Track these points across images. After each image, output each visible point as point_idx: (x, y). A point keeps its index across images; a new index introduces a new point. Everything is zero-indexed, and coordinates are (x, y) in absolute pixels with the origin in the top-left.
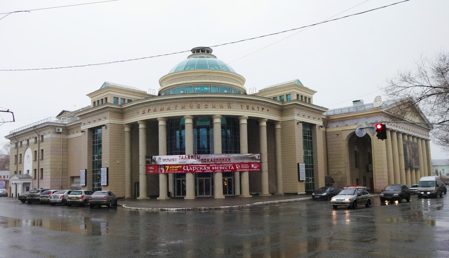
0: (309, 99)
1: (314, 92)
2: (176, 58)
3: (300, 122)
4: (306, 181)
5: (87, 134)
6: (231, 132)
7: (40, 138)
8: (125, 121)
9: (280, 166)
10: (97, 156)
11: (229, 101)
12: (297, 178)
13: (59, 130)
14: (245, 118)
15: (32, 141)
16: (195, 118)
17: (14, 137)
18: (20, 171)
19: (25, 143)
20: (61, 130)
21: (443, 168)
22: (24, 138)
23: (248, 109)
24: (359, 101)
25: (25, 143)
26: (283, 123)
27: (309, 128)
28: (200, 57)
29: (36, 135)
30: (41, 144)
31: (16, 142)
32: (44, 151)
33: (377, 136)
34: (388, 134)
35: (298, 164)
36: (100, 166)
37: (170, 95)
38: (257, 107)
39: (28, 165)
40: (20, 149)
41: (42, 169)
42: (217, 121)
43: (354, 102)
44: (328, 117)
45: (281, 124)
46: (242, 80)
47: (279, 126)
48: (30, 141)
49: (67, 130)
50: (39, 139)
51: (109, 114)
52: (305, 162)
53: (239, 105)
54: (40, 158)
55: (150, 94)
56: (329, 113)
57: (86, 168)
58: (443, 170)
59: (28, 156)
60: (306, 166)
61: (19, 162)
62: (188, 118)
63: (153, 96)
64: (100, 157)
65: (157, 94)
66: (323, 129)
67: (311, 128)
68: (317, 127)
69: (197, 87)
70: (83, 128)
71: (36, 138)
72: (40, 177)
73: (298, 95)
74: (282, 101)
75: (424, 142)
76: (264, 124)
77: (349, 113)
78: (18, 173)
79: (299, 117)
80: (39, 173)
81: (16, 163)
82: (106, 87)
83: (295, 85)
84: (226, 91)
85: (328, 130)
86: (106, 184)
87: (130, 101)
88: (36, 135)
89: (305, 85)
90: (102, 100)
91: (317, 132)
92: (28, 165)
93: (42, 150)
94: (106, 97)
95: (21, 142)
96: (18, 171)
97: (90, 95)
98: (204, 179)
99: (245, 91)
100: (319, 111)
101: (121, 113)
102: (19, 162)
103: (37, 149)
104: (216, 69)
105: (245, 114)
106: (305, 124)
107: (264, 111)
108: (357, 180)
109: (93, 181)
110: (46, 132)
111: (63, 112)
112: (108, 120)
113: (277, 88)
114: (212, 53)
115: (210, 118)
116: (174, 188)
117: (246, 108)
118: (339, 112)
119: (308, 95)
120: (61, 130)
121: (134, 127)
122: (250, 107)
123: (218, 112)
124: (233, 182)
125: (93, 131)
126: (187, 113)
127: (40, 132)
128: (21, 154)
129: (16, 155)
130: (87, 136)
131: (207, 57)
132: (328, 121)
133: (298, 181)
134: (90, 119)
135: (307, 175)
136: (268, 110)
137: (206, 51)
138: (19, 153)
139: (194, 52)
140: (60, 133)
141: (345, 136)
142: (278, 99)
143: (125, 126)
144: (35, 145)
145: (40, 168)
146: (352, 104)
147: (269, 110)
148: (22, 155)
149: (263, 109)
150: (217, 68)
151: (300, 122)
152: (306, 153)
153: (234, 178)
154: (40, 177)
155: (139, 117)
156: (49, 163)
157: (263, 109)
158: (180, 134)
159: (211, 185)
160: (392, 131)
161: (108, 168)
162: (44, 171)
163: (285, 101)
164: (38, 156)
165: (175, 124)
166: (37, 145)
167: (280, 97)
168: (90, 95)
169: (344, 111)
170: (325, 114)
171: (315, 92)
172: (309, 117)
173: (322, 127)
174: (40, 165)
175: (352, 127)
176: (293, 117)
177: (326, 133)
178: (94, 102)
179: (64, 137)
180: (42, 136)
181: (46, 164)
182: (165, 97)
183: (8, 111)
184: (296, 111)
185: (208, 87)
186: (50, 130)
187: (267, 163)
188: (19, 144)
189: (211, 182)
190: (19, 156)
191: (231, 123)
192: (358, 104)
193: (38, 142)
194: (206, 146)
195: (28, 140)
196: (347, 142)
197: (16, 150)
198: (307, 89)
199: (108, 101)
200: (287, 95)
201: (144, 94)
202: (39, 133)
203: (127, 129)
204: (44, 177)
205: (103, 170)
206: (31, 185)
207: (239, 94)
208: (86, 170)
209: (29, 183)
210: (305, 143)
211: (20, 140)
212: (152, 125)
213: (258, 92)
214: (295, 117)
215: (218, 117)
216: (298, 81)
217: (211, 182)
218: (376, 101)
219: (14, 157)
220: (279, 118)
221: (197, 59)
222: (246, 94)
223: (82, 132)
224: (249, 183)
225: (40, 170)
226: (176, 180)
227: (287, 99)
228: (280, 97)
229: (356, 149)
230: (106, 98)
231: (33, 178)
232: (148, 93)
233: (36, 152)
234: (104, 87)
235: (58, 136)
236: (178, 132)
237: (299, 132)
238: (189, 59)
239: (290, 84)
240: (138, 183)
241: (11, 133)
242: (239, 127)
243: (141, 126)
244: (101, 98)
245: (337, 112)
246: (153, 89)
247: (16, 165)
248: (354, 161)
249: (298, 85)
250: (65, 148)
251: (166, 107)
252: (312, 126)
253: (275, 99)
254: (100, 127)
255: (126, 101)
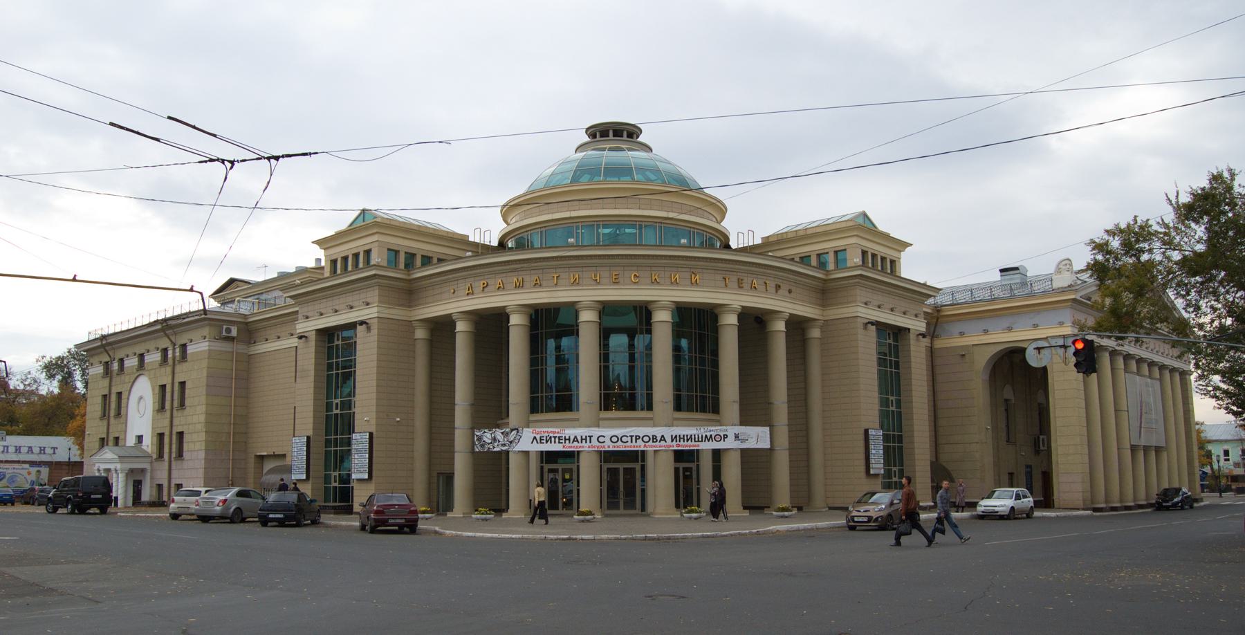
0: (892, 262)
1: (906, 245)
2: (552, 147)
3: (872, 323)
4: (884, 476)
5: (312, 343)
6: (689, 344)
7: (178, 350)
8: (417, 312)
9: (817, 436)
10: (338, 401)
11: (693, 267)
12: (863, 468)
13: (229, 331)
14: (733, 311)
15: (153, 358)
16: (606, 309)
17: (103, 346)
18: (117, 439)
19: (131, 363)
20: (234, 333)
21: (1226, 447)
22: (129, 351)
23: (740, 287)
24: (1017, 269)
25: (131, 363)
26: (826, 325)
27: (892, 336)
28: (611, 149)
29: (164, 343)
30: (178, 368)
31: (107, 359)
32: (188, 385)
33: (1076, 365)
34: (1105, 359)
35: (866, 431)
36: (350, 429)
37: (533, 248)
38: (762, 282)
39: (141, 420)
40: (116, 380)
41: (181, 434)
42: (662, 317)
43: (1001, 271)
44: (938, 309)
45: (821, 327)
46: (720, 209)
47: (815, 333)
48: (148, 359)
49: (249, 331)
50: (174, 352)
51: (377, 292)
52: (882, 427)
53: (719, 277)
54: (176, 404)
55: (477, 240)
56: (941, 299)
57: (310, 433)
58: (1226, 453)
59: (141, 398)
60: (886, 438)
61: (112, 413)
62: (588, 308)
63: (484, 249)
64: (347, 405)
65: (495, 243)
66: (925, 342)
67: (896, 340)
68: (912, 336)
69: (605, 227)
70: (302, 327)
71: (165, 351)
72: (174, 455)
73: (864, 253)
74: (822, 265)
75: (1177, 377)
76: (780, 326)
77: (993, 300)
78: (111, 442)
79: (864, 309)
80: (171, 444)
81: (105, 415)
82: (366, 223)
83: (858, 227)
84: (683, 241)
85: (939, 344)
86: (366, 476)
87: (427, 260)
88: (164, 343)
89: (882, 227)
90: (356, 256)
91: (912, 348)
92: (141, 420)
93: (183, 384)
94: (367, 248)
95: (122, 361)
96: (111, 438)
97: (321, 243)
98: (621, 466)
99: (727, 238)
100: (918, 293)
101: (409, 293)
102: (112, 413)
103: (167, 380)
104: (649, 181)
105: (732, 300)
106: (881, 327)
107: (780, 292)
108: (1011, 474)
109: (327, 468)
110: (195, 335)
111: (232, 281)
112: (376, 309)
113: (809, 232)
114: (641, 139)
115: (644, 312)
116: (698, 483)
117: (774, 290)
118: (965, 297)
119: (889, 253)
120: (234, 333)
121: (442, 328)
122: (747, 281)
123: (665, 295)
124: (695, 476)
125: (327, 335)
126: (585, 295)
127: (175, 334)
128: (120, 394)
129: (105, 396)
130: (313, 350)
131: (630, 150)
132: (937, 320)
133: (863, 474)
134: (323, 305)
135: (887, 462)
136: (790, 292)
137: (625, 134)
138: (115, 390)
139: (593, 136)
140: (233, 339)
141: (982, 360)
142: (814, 262)
143: (415, 324)
144: (163, 369)
145: (176, 430)
146: (996, 276)
147: (794, 289)
148: (124, 396)
149: (778, 287)
150: (652, 177)
151: (872, 323)
152: (884, 403)
153: (643, 468)
154: (174, 455)
155: (456, 304)
156: (202, 418)
157: (778, 287)
158: (558, 348)
159: (695, 481)
160: (1113, 353)
161: (371, 435)
162: (186, 438)
163: (831, 266)
164: (170, 399)
165: (550, 324)
166: (169, 369)
167: (819, 255)
168: (321, 243)
169: (979, 295)
170: (930, 301)
171: (907, 245)
172: (892, 310)
173: (924, 336)
174: (176, 422)
175: (1001, 336)
176: (851, 310)
177: (931, 351)
178: (334, 262)
179: (240, 348)
180: (184, 346)
181: (194, 420)
182: (517, 249)
183: (191, 290)
184: (861, 294)
185: (633, 227)
186: (206, 331)
187: (785, 429)
188: (116, 366)
189: (638, 475)
190: (114, 398)
191: (696, 323)
192: (1015, 278)
193: (170, 361)
194: (624, 380)
195: (142, 356)
196: (987, 377)
197: (106, 381)
198: (886, 236)
199: (375, 259)
200: (836, 252)
201: (461, 242)
202: (173, 338)
203: (421, 334)
204: (186, 455)
205: (359, 440)
206: (148, 475)
207: (711, 246)
208: (308, 438)
209: (143, 471)
210: (882, 376)
211: (118, 356)
212: (491, 326)
213: (760, 242)
214: (860, 309)
215: (664, 308)
216: (865, 215)
217: (638, 475)
218: (1058, 271)
219: (99, 400)
220: (817, 312)
221: (607, 155)
222: (727, 247)
223: (300, 338)
224: (742, 480)
225: (174, 437)
226: (546, 470)
227: (837, 262)
228: (819, 255)
229: (1008, 393)
230: (368, 252)
231: (155, 456)
232: (471, 239)
233: (163, 387)
234: (359, 223)
235: (226, 347)
236: (551, 343)
237: (867, 348)
238: (580, 155)
239: (844, 225)
240: (449, 478)
241: (92, 337)
242: (717, 332)
243: (461, 326)
244: (355, 251)
245: (960, 298)
246: (487, 227)
247: (105, 422)
248: (1003, 425)
249: (863, 225)
250: (238, 383)
251: (530, 278)
252: (899, 333)
253: (804, 260)
254: (352, 326)
255: (418, 261)
